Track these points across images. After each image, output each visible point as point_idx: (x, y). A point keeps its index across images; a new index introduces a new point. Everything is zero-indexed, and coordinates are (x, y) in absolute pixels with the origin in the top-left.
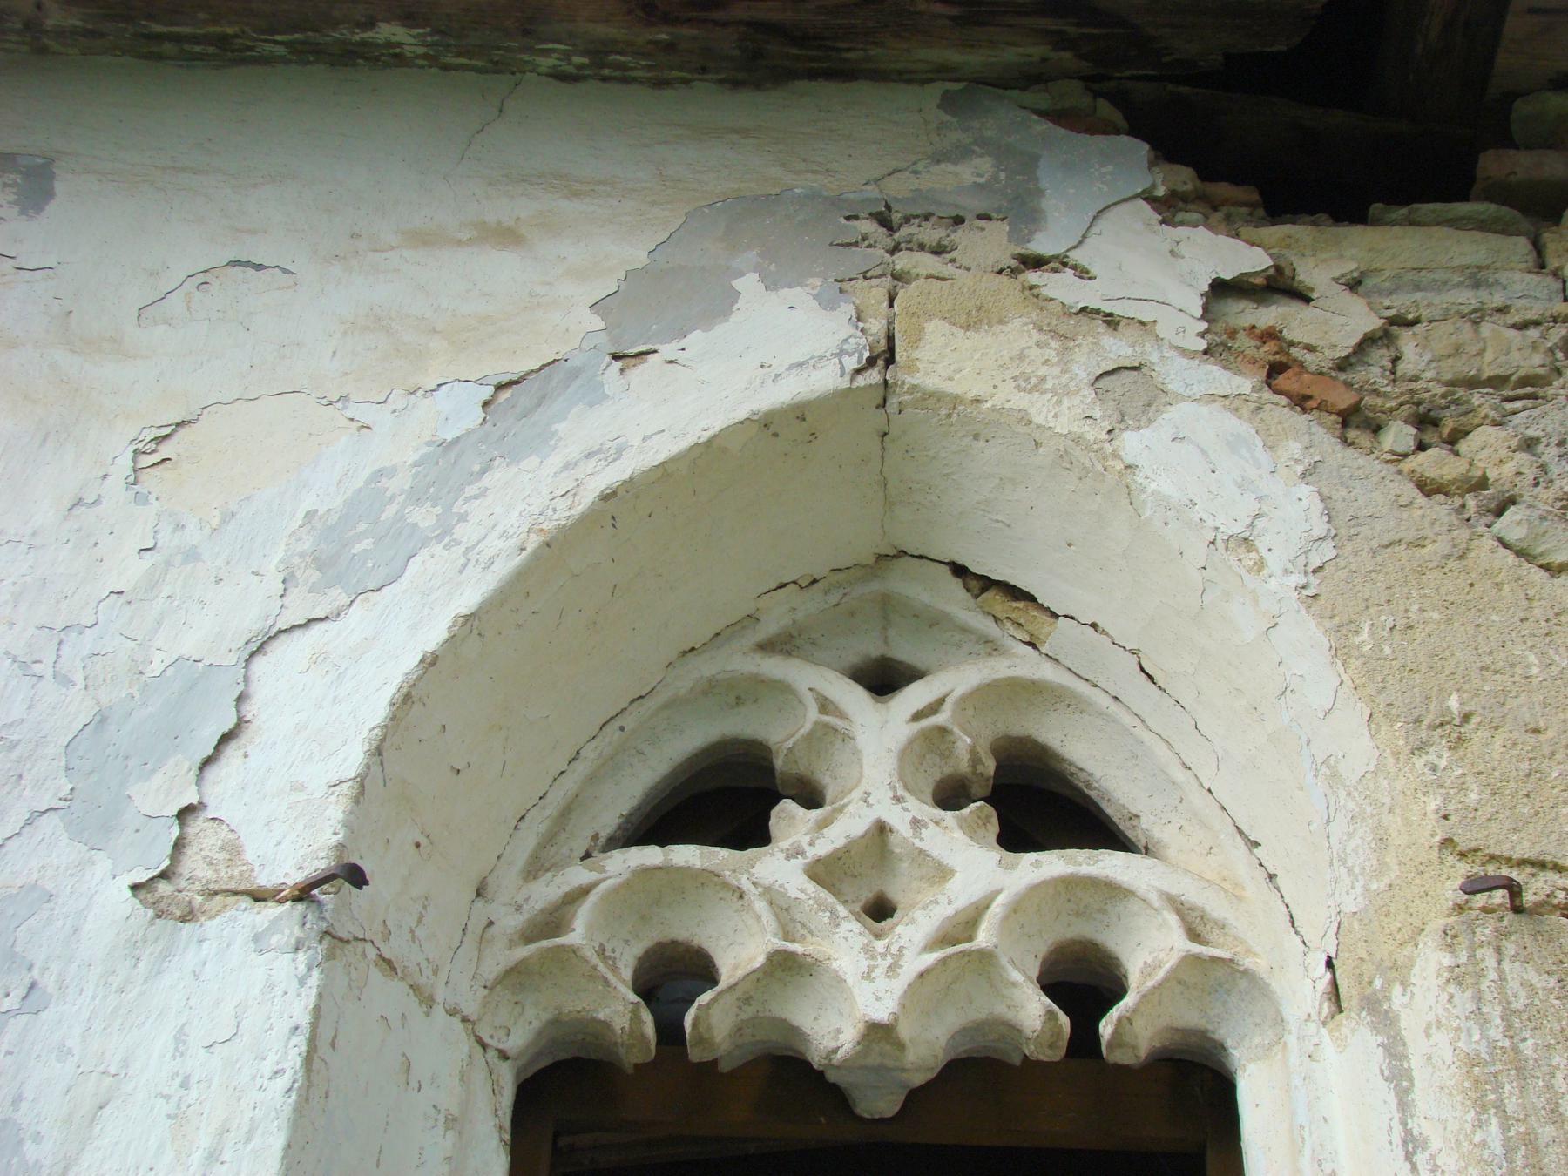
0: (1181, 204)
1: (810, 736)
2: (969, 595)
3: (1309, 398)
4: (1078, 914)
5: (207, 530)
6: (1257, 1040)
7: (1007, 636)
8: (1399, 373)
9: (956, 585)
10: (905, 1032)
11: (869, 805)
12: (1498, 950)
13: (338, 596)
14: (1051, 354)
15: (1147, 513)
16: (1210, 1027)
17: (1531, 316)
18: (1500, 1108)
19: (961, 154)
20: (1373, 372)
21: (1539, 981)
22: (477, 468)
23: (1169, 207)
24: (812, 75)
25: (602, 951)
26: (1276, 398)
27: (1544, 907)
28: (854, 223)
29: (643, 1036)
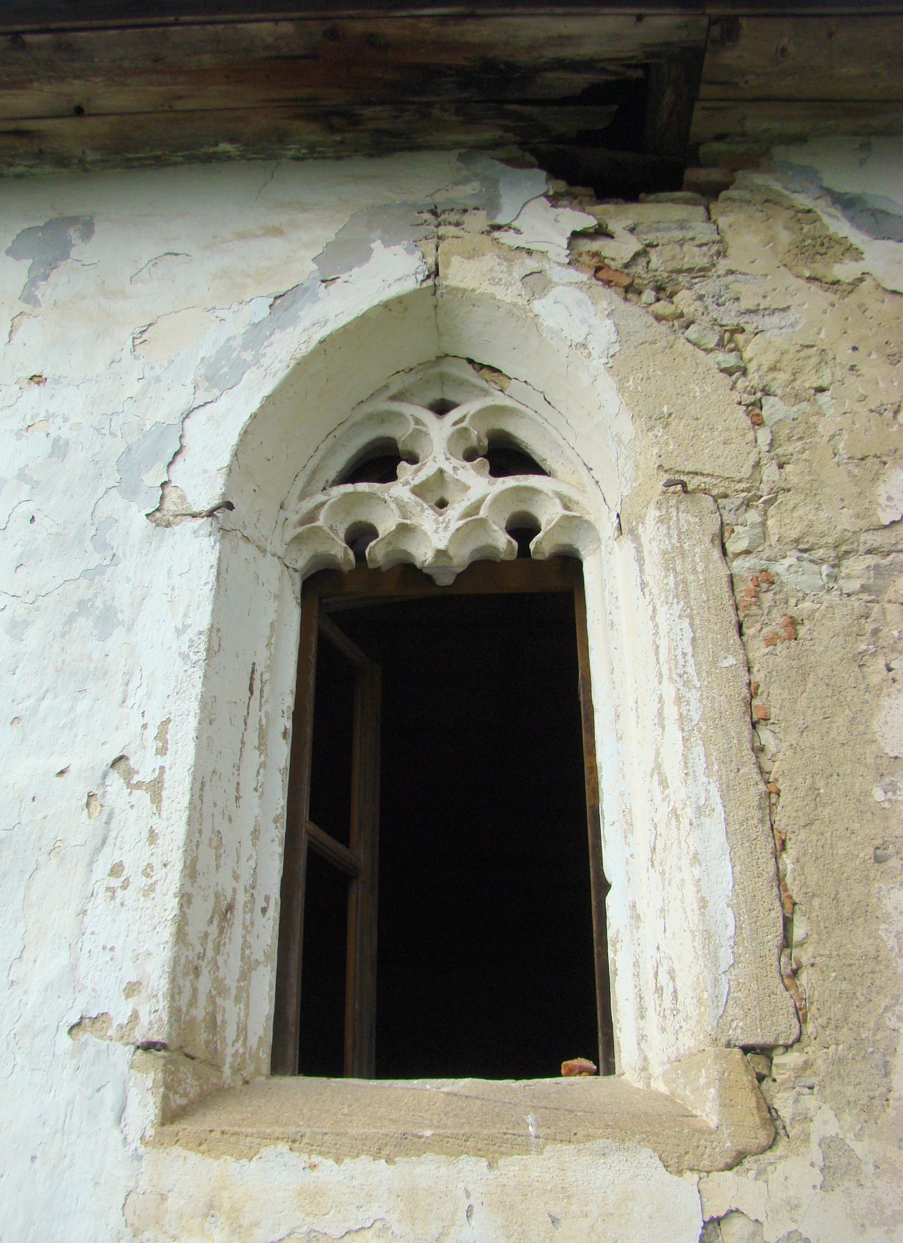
0: (560, 198)
1: (411, 435)
2: (475, 371)
3: (612, 281)
4: (521, 501)
5: (163, 368)
6: (591, 547)
7: (493, 388)
8: (650, 268)
9: (470, 367)
10: (451, 552)
11: (435, 462)
12: (677, 508)
13: (216, 392)
14: (505, 269)
15: (544, 335)
16: (573, 543)
17: (704, 241)
18: (674, 570)
19: (466, 181)
20: (639, 269)
21: (692, 520)
22: (268, 334)
23: (554, 200)
24: (402, 150)
25: (331, 528)
26: (598, 282)
27: (694, 492)
28: (422, 215)
29: (350, 560)
